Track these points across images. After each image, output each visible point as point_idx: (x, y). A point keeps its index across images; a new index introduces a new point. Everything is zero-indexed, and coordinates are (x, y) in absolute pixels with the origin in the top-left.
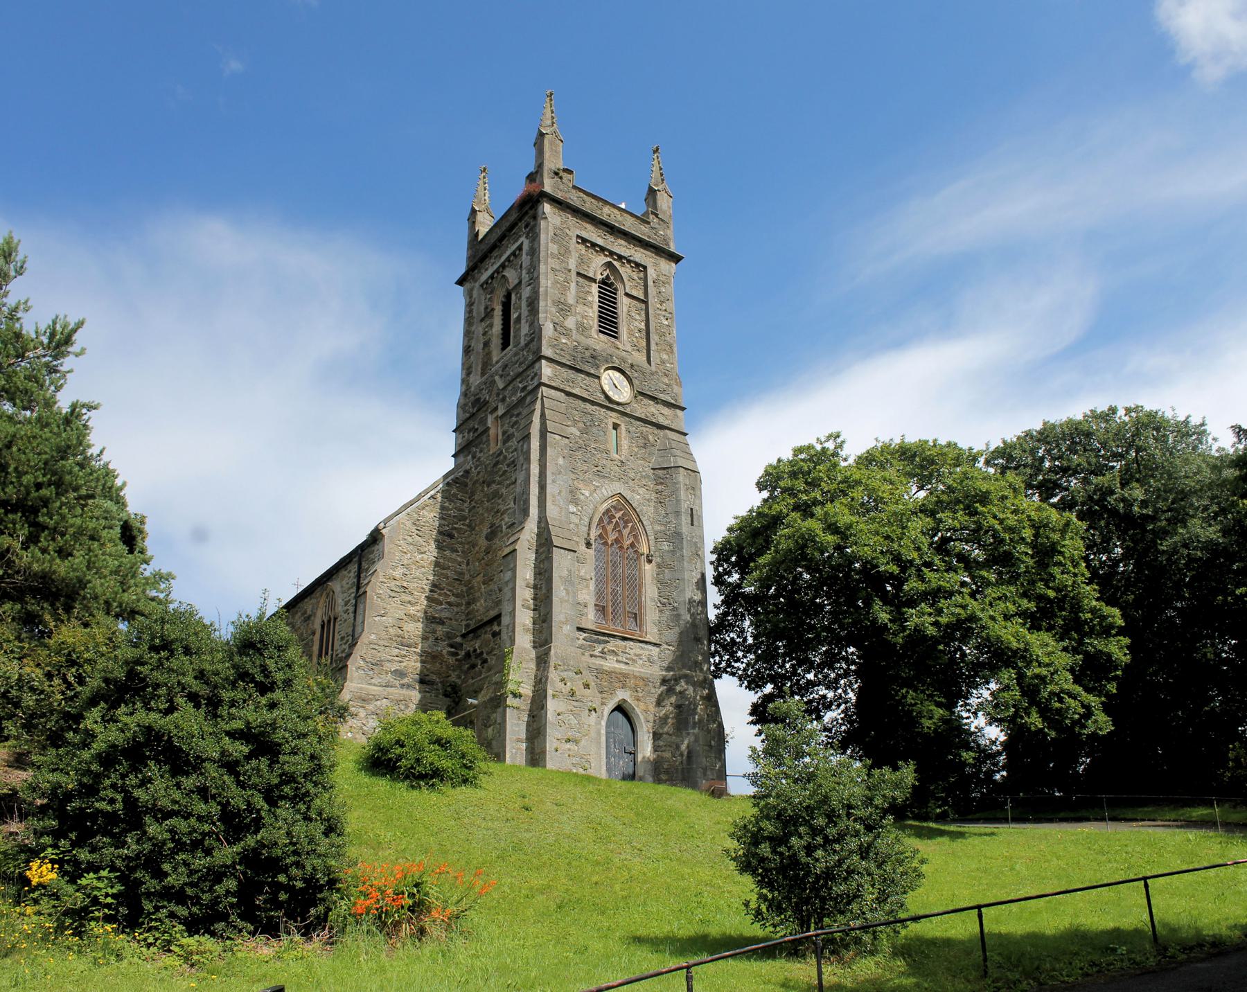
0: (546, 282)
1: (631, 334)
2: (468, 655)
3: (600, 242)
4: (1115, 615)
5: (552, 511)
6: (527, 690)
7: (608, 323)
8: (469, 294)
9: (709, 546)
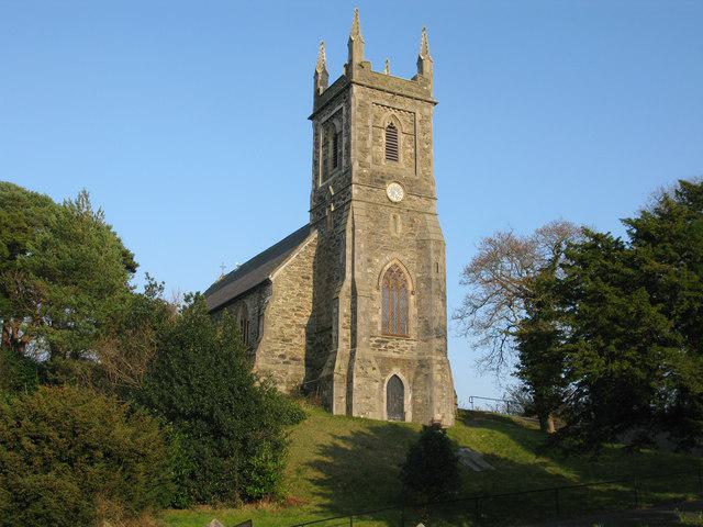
0: (354, 138)
1: (405, 156)
2: (318, 345)
3: (348, 301)
4: (680, 338)
5: (358, 275)
6: (344, 371)
7: (392, 153)
8: (316, 127)
9: (458, 255)
